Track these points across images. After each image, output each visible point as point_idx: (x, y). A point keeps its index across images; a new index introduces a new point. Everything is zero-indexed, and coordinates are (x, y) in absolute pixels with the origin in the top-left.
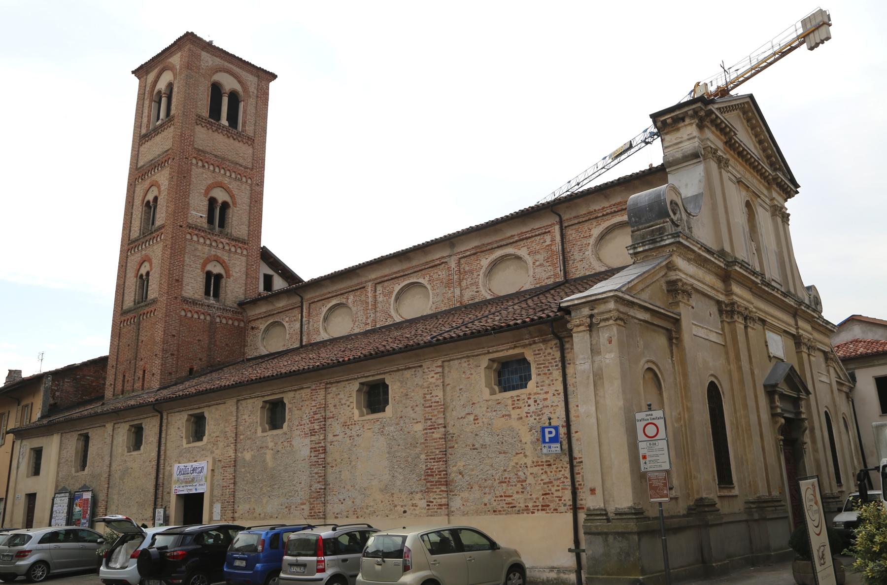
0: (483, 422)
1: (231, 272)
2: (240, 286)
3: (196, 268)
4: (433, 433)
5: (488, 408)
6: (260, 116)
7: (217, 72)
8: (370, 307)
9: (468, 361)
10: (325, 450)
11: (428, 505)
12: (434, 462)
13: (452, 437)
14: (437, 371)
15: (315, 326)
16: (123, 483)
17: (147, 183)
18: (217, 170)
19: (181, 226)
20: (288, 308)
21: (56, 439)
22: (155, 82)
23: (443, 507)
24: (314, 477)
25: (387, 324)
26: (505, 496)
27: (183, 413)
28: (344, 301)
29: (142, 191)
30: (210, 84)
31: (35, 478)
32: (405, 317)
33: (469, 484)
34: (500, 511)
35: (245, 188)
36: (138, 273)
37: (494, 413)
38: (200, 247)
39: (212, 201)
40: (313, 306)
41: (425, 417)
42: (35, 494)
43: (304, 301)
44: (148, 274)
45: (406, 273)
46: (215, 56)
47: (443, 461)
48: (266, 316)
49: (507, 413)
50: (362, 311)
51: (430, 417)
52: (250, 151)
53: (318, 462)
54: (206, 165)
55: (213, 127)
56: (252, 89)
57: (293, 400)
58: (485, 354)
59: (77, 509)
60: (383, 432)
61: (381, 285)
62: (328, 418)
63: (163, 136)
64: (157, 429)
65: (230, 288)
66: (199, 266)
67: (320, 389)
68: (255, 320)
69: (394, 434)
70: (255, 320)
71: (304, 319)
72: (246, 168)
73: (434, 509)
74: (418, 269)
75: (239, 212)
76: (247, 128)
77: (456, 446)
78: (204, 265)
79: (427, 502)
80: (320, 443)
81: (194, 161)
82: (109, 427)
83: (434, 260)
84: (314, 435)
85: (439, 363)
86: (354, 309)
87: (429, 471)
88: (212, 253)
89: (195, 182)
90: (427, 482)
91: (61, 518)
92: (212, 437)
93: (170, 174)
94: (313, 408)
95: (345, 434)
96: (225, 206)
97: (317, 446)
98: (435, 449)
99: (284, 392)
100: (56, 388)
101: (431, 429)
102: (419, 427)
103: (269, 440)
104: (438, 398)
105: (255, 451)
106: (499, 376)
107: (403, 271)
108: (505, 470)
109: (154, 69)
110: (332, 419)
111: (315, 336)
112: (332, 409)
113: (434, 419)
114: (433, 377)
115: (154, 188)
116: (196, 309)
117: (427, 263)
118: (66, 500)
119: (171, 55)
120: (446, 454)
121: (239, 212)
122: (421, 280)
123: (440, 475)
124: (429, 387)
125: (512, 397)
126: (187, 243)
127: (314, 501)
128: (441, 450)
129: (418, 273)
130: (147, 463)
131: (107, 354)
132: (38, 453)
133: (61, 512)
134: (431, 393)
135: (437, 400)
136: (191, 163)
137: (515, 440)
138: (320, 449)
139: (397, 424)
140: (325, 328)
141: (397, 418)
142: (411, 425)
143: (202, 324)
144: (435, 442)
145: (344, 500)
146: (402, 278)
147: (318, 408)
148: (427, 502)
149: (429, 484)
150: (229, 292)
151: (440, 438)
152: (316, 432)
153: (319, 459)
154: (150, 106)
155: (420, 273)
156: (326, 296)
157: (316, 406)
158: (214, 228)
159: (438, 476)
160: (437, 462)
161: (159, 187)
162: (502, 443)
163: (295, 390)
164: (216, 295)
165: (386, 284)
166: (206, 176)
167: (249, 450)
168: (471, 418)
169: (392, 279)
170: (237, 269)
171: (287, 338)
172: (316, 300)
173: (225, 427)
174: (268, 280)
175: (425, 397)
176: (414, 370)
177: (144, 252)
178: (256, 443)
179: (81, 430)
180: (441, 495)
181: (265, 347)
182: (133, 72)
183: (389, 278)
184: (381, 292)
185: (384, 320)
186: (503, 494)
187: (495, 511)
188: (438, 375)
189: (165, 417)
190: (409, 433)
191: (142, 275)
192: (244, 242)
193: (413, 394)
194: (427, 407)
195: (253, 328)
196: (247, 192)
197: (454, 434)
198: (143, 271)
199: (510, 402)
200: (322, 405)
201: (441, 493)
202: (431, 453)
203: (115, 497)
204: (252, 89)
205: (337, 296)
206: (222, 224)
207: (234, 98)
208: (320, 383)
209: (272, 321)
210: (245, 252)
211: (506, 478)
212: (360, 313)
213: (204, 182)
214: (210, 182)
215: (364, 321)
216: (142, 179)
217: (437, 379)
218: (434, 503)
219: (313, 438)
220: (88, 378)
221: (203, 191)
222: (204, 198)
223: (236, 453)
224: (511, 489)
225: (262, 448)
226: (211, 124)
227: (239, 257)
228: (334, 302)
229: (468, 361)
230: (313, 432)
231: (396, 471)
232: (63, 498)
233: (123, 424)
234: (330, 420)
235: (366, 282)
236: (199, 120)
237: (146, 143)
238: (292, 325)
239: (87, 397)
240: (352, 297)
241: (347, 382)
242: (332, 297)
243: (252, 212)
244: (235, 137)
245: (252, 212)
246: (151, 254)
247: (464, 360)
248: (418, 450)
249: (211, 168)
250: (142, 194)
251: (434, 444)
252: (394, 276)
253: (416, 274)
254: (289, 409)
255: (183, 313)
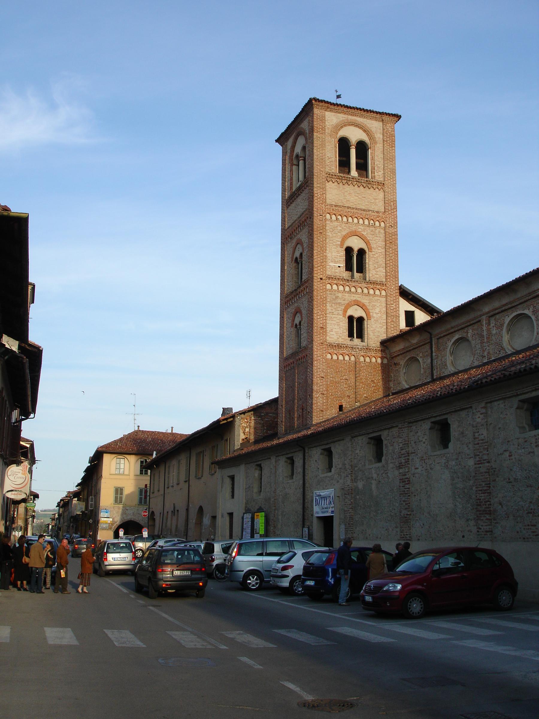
0: (515, 458)
1: (371, 314)
2: (381, 325)
3: (338, 314)
4: (480, 467)
5: (518, 446)
6: (388, 160)
7: (342, 127)
8: (485, 340)
9: (504, 402)
10: (409, 481)
11: (478, 531)
12: (481, 493)
13: (494, 471)
14: (482, 412)
15: (443, 360)
17: (294, 241)
18: (350, 219)
19: (321, 279)
20: (421, 344)
21: (242, 468)
22: (293, 147)
23: (488, 533)
24: (402, 504)
25: (500, 356)
26: (532, 526)
28: (464, 335)
29: (291, 249)
30: (337, 140)
31: (233, 500)
32: (515, 348)
33: (506, 514)
34: (528, 538)
35: (379, 232)
36: (293, 324)
37: (523, 450)
38: (340, 295)
39: (349, 251)
40: (440, 340)
41: (475, 453)
42: (233, 513)
43: (432, 336)
44: (300, 323)
45: (513, 305)
46: (339, 113)
47: (488, 493)
48: (405, 353)
49: (532, 451)
50: (479, 345)
51: (478, 453)
52: (381, 195)
53: (405, 491)
54: (339, 217)
55: (343, 181)
56: (379, 136)
57: (387, 437)
58: (515, 396)
60: (447, 466)
61: (493, 318)
62: (411, 453)
63: (302, 197)
64: (301, 461)
65: (372, 329)
66: (341, 313)
67: (404, 428)
68: (396, 356)
69: (455, 468)
70: (396, 356)
71: (434, 354)
72: (378, 212)
73: (482, 535)
74: (523, 300)
75: (375, 256)
76: (376, 174)
77: (497, 479)
78: (345, 311)
79: (477, 528)
80: (406, 475)
81: (328, 216)
82: (273, 459)
83: (535, 291)
84: (402, 468)
85: (483, 405)
86: (473, 342)
87: (478, 501)
88: (352, 298)
89: (331, 235)
90: (477, 511)
92: (337, 469)
93: (309, 232)
94: (400, 444)
95: (423, 467)
96: (361, 253)
97: (404, 477)
98: (482, 482)
99: (381, 430)
100: (245, 425)
101: (479, 464)
102: (471, 462)
103: (373, 471)
104: (483, 436)
105: (365, 481)
106: (531, 415)
107: (510, 303)
108: (531, 502)
109: (291, 136)
110: (414, 454)
111: (443, 370)
112: (414, 445)
113: (481, 454)
114: (479, 417)
115: (299, 246)
116: (341, 352)
117: (530, 294)
119: (300, 123)
120: (490, 487)
121: (375, 256)
122: (526, 312)
123: (486, 505)
124: (477, 427)
125: (535, 436)
126: (328, 292)
127: (403, 525)
128: (486, 483)
129: (523, 305)
131: (275, 394)
132: (232, 478)
134: (478, 432)
135: (483, 438)
136: (326, 220)
137: (537, 475)
138: (406, 480)
139: (457, 459)
140: (452, 362)
141: (456, 454)
142: (466, 460)
143: (348, 364)
144: (482, 476)
145: (423, 524)
146: (510, 311)
147: (403, 445)
148: (477, 528)
149: (478, 513)
150: (370, 333)
151: (485, 472)
152: (403, 465)
153: (405, 489)
154: (291, 170)
155: (525, 305)
156: (450, 331)
157: (402, 442)
158: (352, 276)
159: (484, 506)
160: (484, 493)
161: (302, 245)
162: (529, 477)
163: (389, 429)
164: (360, 336)
165: (497, 316)
166: (341, 228)
167: (361, 481)
168: (507, 454)
169: (502, 311)
170: (377, 310)
171: (422, 373)
172: (442, 335)
173: (345, 460)
174: (410, 316)
175: (474, 436)
176: (467, 410)
177: (296, 305)
178: (365, 474)
180: (486, 522)
181: (406, 381)
182: (277, 141)
183: (500, 310)
184: (493, 325)
185: (498, 353)
186: (529, 524)
187: (524, 538)
188: (483, 415)
189: (307, 451)
190: (465, 467)
191: (296, 325)
192: (381, 284)
193: (467, 432)
194: (476, 444)
195: (395, 364)
196: (382, 236)
197: (496, 469)
198: (297, 321)
199: (533, 440)
200: (406, 441)
201: (487, 521)
202: (480, 485)
203: (280, 517)
204: (379, 136)
205: (458, 330)
206: (361, 269)
207: (362, 148)
208: (404, 423)
209: (409, 357)
210: (383, 293)
211: (531, 509)
212: (479, 346)
213: (339, 234)
214: (344, 233)
215: (481, 354)
216: (291, 238)
217: (482, 420)
218: (482, 530)
219: (401, 471)
220: (270, 415)
221: (339, 243)
222: (339, 248)
223: (405, 481)
224: (535, 519)
225: (370, 478)
226: (341, 179)
227: (378, 298)
228: (457, 337)
229: (504, 402)
230: (400, 467)
231: (457, 501)
233: (281, 457)
234: (412, 455)
235: (481, 316)
236: (330, 177)
237: (291, 205)
238: (425, 361)
239: (271, 432)
240: (470, 331)
241: (422, 422)
242: (455, 332)
243: (388, 253)
244: (365, 185)
245: (388, 253)
246: (301, 305)
247: (501, 402)
248: (471, 482)
249: (345, 219)
250: (291, 252)
251: (481, 477)
252: (504, 308)
253: (522, 305)
254: (385, 445)
255: (329, 356)
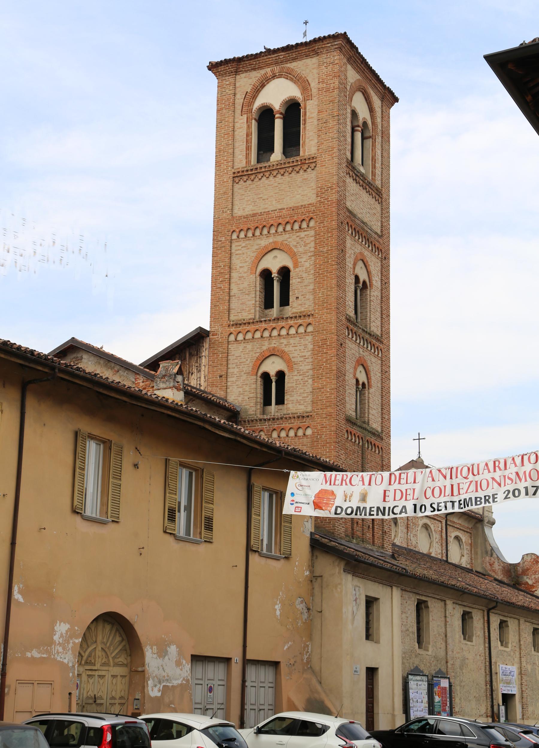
16: (463, 673)
27: (497, 615)
59: (437, 699)
91: (420, 709)
118: (424, 686)
130: (478, 657)
133: (420, 700)
179: (422, 595)
232: (420, 683)
